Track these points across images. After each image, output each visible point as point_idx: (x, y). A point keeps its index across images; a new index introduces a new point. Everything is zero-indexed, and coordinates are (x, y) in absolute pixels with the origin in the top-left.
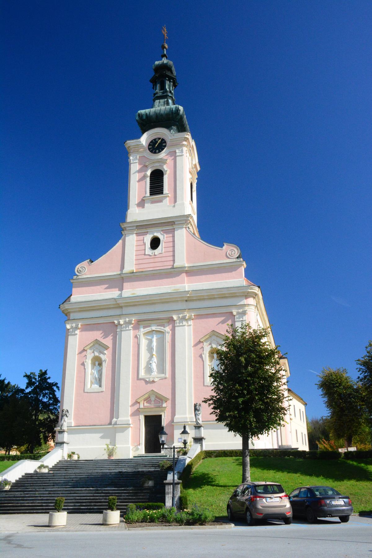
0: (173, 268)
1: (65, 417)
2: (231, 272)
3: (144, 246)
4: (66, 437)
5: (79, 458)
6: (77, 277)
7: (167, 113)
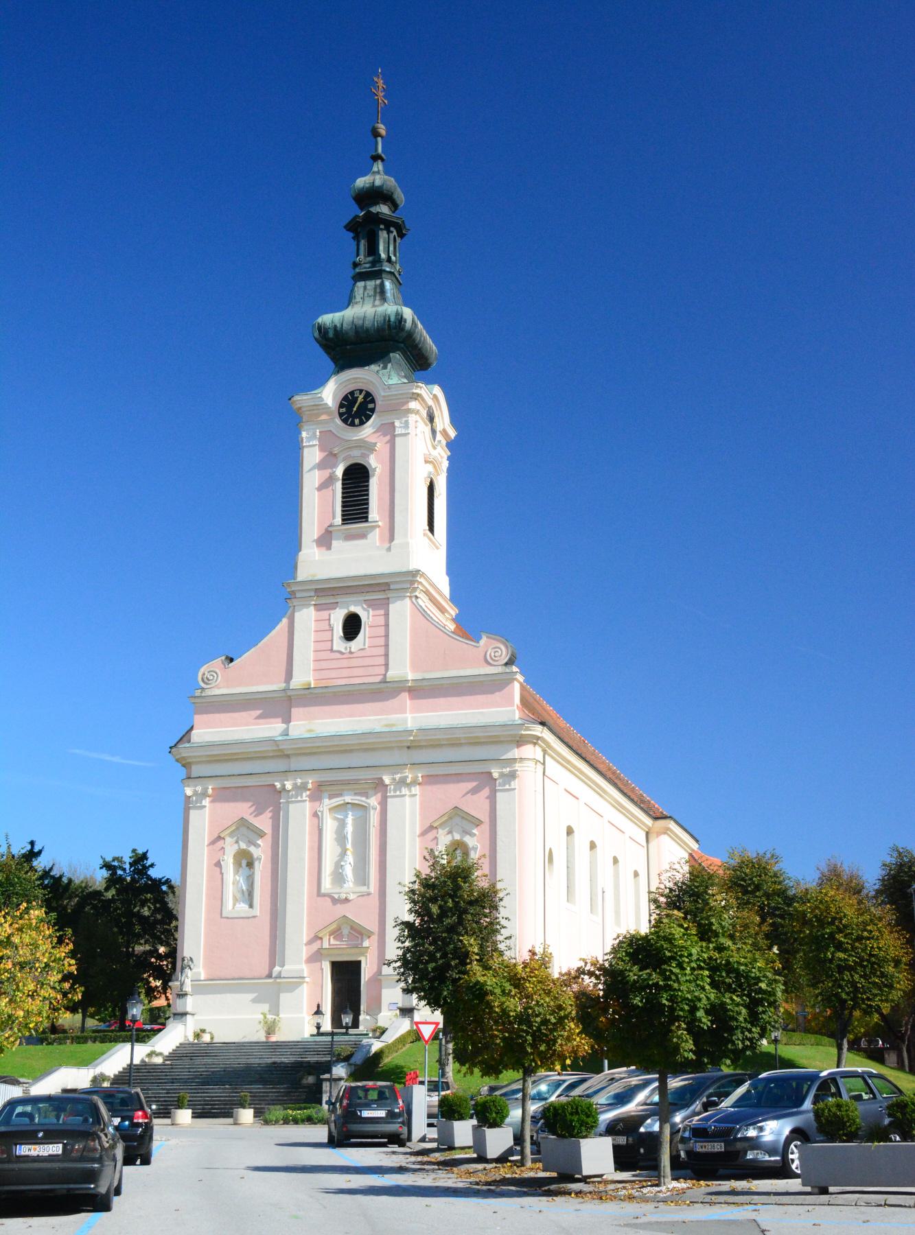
0: (384, 681)
1: (187, 970)
2: (492, 692)
3: (331, 632)
4: (190, 1004)
5: (212, 1038)
6: (201, 693)
7: (378, 326)
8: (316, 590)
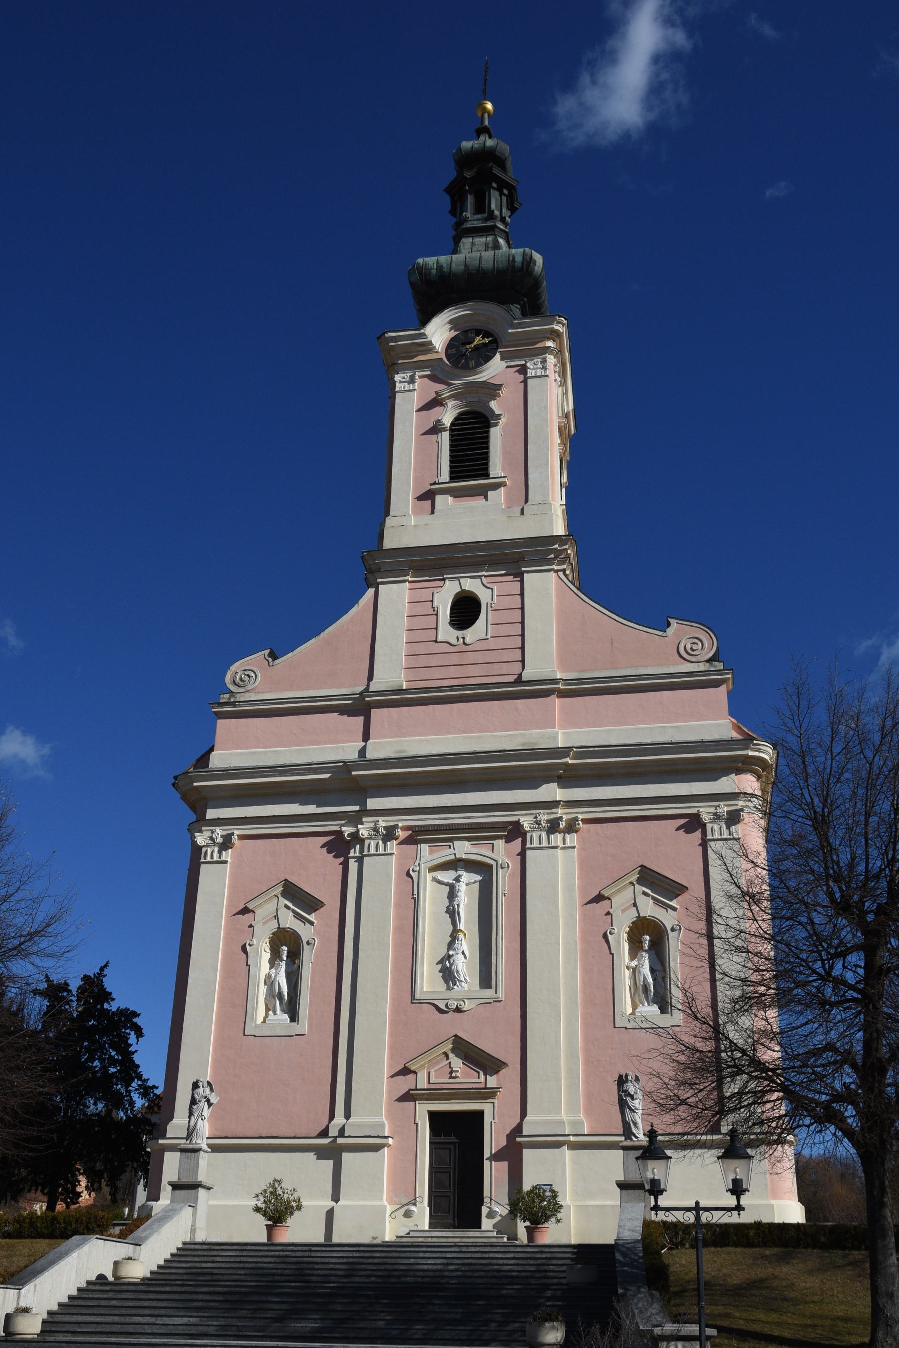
7: (498, 266)
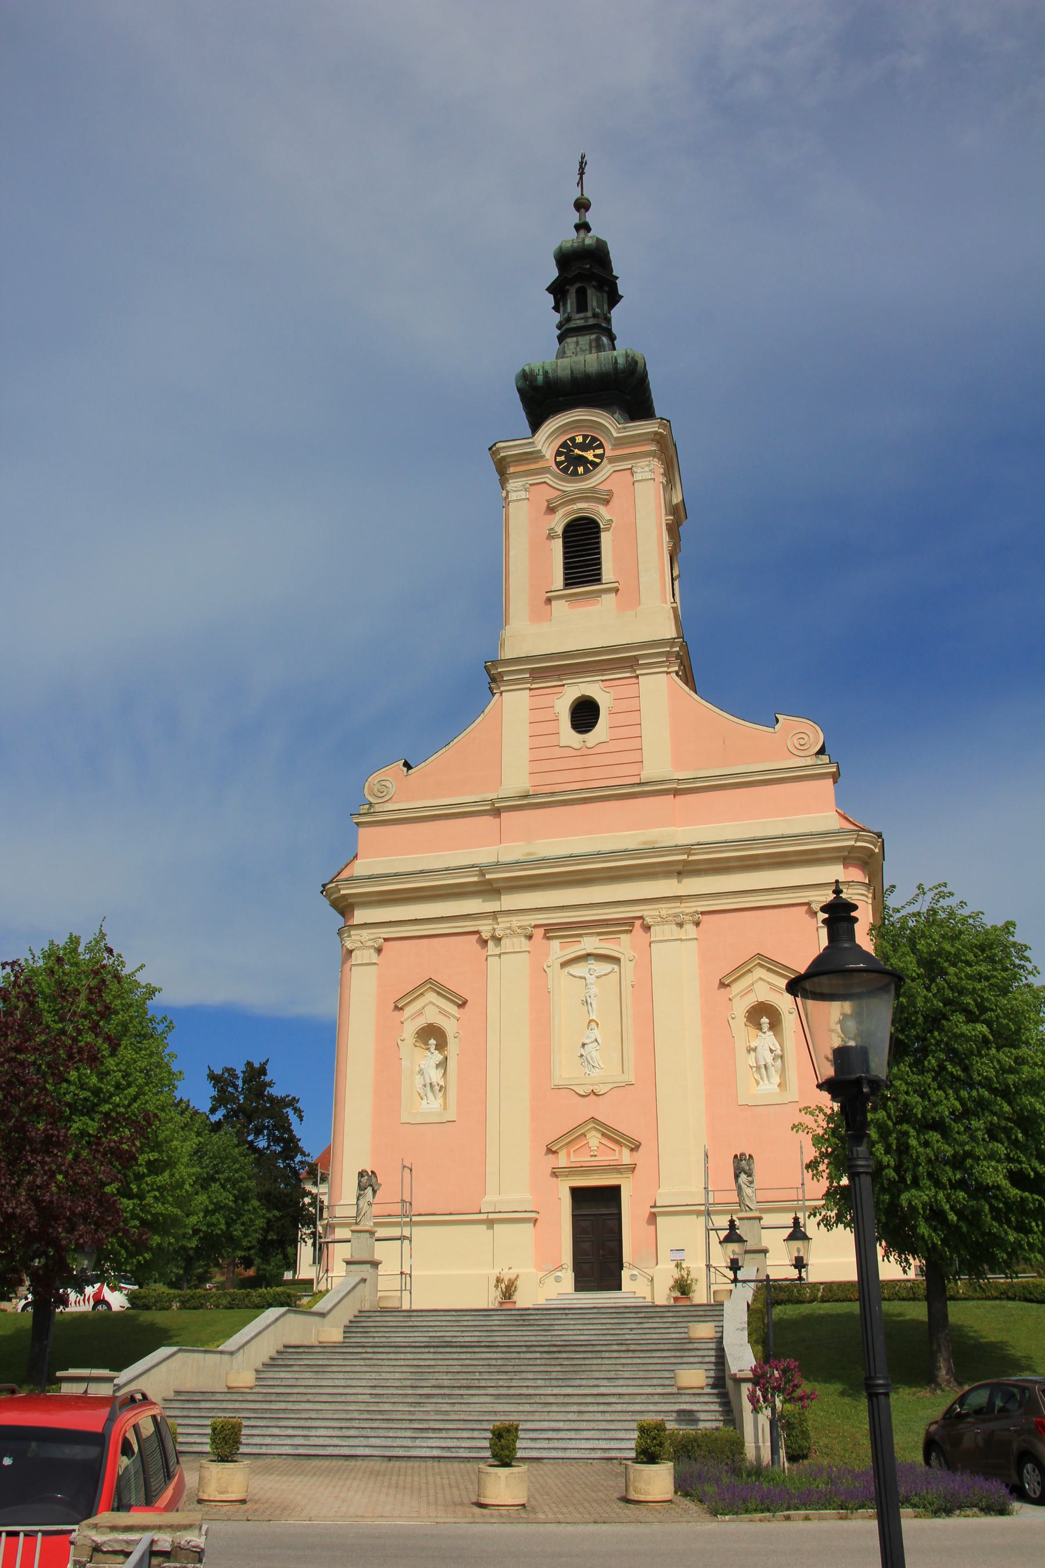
8: (532, 671)
